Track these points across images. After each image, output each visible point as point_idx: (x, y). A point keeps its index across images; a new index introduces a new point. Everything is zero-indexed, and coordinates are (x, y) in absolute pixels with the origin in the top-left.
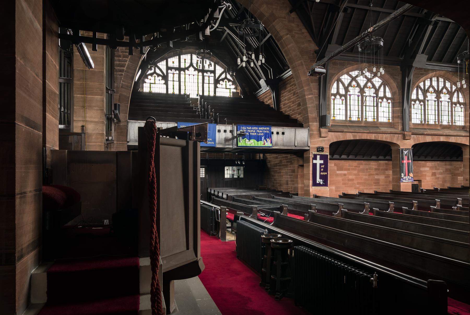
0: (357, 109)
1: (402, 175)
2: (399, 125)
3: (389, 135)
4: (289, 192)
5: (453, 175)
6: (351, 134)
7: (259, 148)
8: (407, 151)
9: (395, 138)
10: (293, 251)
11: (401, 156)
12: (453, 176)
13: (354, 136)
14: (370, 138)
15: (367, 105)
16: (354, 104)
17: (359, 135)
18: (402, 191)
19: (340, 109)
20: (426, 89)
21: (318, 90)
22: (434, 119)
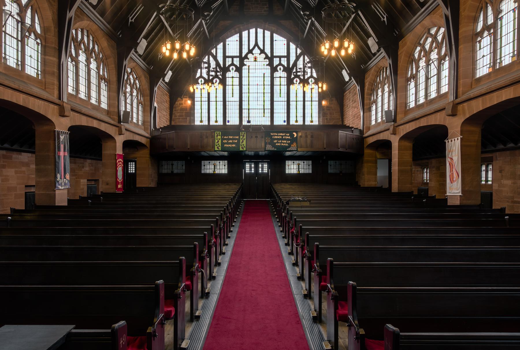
0: (253, 89)
1: (59, 176)
2: (54, 89)
5: (77, 177)
8: (64, 136)
10: (154, 286)
11: (58, 143)
12: (76, 178)
15: (311, 102)
18: (56, 205)
21: (403, 123)
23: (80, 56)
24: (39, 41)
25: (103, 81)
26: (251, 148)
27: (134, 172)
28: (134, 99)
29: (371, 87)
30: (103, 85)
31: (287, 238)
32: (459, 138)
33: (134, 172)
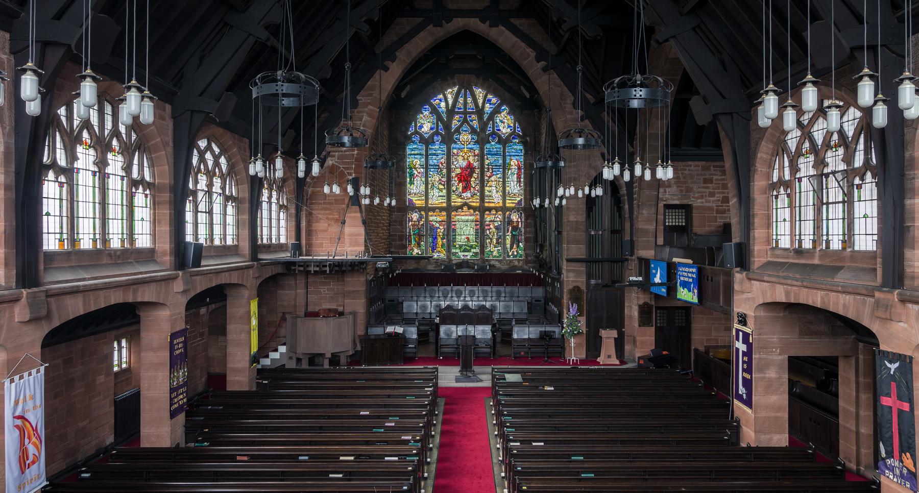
3: (852, 297)
4: (322, 352)
6: (781, 287)
7: (140, 276)
9: (867, 310)
13: (787, 293)
14: (813, 303)
16: (116, 206)
17: (794, 292)
19: (865, 216)
20: (57, 132)
22: (92, 231)
23: (109, 165)
24: (148, 192)
25: (141, 189)
26: (514, 301)
27: (684, 224)
28: (200, 200)
29: (769, 157)
30: (141, 199)
31: (356, 460)
32: (42, 369)
33: (684, 224)
